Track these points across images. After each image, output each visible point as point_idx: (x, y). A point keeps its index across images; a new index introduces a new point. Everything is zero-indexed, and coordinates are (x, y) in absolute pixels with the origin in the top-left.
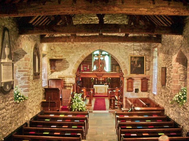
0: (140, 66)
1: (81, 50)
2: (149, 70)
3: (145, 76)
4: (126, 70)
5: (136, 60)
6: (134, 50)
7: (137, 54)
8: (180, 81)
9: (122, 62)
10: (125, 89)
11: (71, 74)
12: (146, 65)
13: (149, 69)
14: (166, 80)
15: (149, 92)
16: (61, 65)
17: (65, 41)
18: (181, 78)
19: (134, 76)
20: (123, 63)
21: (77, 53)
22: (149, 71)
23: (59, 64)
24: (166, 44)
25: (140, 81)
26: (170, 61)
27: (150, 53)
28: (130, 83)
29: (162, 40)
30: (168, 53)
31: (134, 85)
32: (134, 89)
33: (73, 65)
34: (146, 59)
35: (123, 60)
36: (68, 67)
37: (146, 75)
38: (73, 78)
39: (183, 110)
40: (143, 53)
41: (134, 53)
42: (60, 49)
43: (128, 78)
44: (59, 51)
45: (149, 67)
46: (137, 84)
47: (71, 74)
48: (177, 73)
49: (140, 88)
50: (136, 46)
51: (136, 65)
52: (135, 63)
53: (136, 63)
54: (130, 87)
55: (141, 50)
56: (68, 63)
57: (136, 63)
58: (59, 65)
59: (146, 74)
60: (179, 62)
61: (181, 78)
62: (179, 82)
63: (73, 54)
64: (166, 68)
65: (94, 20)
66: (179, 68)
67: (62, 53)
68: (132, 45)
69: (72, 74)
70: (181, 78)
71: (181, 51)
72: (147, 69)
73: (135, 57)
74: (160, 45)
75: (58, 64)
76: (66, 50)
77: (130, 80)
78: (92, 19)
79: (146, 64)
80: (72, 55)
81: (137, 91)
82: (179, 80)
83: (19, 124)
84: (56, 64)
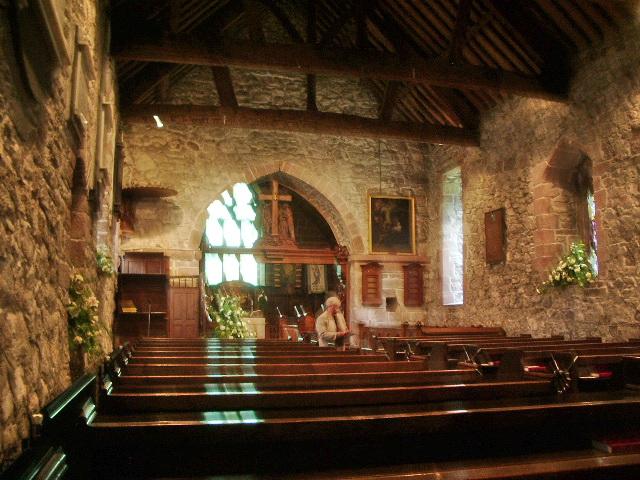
0: (399, 228)
1: (220, 172)
2: (424, 240)
3: (415, 259)
4: (359, 240)
5: (387, 210)
6: (381, 180)
7: (389, 190)
8: (558, 232)
9: (346, 213)
10: (356, 298)
11: (186, 247)
12: (416, 227)
13: (426, 238)
14: (504, 242)
15: (427, 310)
16: (154, 217)
17: (202, 121)
18: (560, 226)
19: (383, 256)
20: (350, 216)
21: (208, 180)
22: (424, 245)
23: (148, 211)
24: (502, 143)
25: (400, 273)
26: (520, 185)
27: (426, 188)
28: (371, 280)
29: (484, 137)
30: (510, 166)
31: (385, 288)
32: (384, 298)
33: (196, 219)
34: (415, 206)
35: (351, 208)
36: (25, 302)
37: (417, 254)
38: (194, 260)
39: (585, 301)
40: (408, 189)
41: (383, 187)
42: (151, 165)
43: (364, 264)
44: (149, 171)
45: (425, 232)
46: (392, 282)
47: (186, 247)
48: (549, 212)
49: (399, 293)
50: (387, 167)
51: (388, 225)
52: (384, 219)
53: (388, 217)
54: (372, 291)
55: (401, 181)
56: (176, 212)
57: (388, 217)
58: (149, 215)
59: (417, 250)
60: (553, 181)
61: (561, 223)
62: (556, 235)
63: (195, 184)
64: (502, 211)
65: (263, 80)
66: (553, 197)
67: (158, 176)
68: (375, 165)
69: (190, 246)
70: (561, 223)
71: (564, 145)
72: (420, 237)
73: (385, 201)
74: (472, 152)
75: (143, 212)
76: (172, 168)
77: (372, 268)
78: (255, 78)
79: (416, 222)
80: (191, 184)
81: (391, 302)
82: (555, 230)
83: (336, 227)
84: (138, 212)
